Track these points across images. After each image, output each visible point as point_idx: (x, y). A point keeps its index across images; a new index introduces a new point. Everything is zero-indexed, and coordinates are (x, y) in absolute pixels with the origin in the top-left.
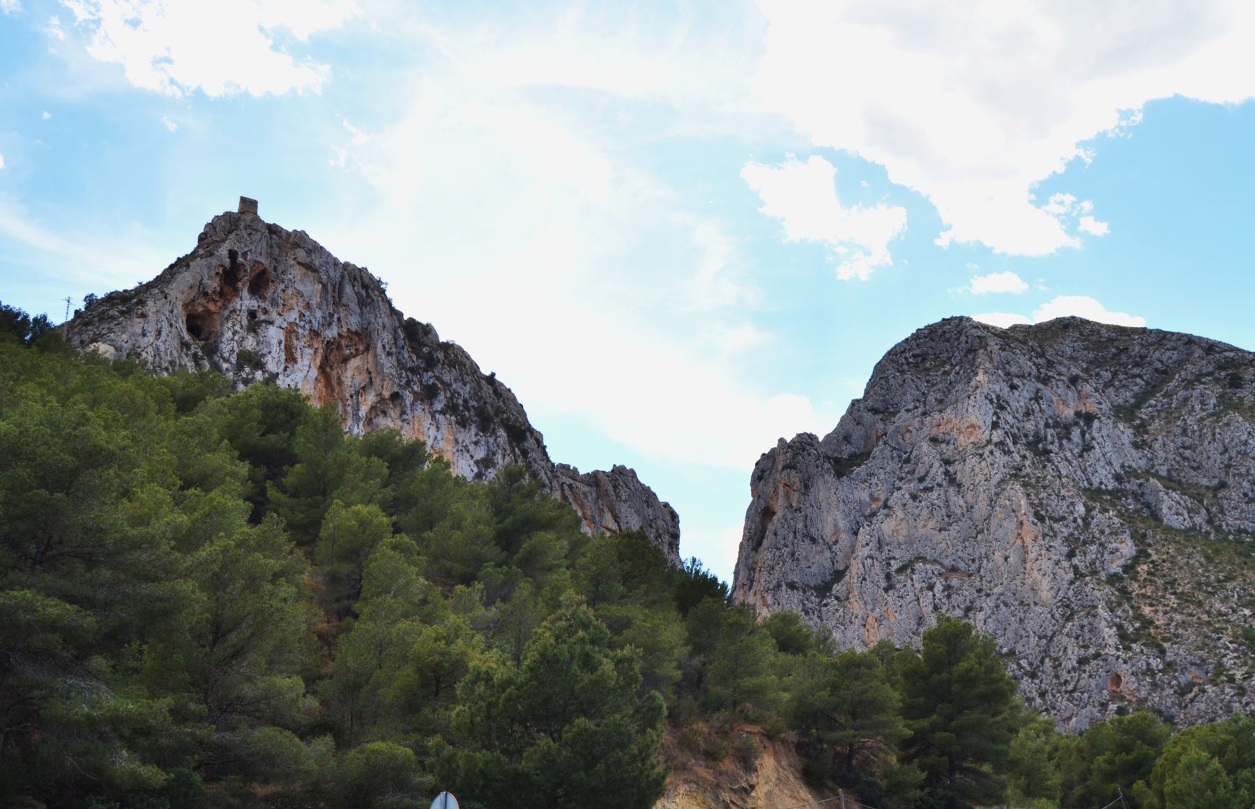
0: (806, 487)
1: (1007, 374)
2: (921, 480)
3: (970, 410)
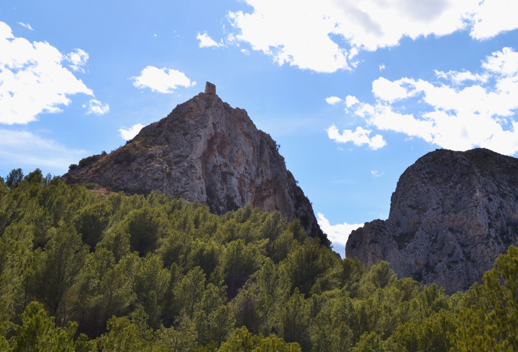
0: (384, 254)
1: (487, 191)
2: (450, 256)
3: (478, 215)
